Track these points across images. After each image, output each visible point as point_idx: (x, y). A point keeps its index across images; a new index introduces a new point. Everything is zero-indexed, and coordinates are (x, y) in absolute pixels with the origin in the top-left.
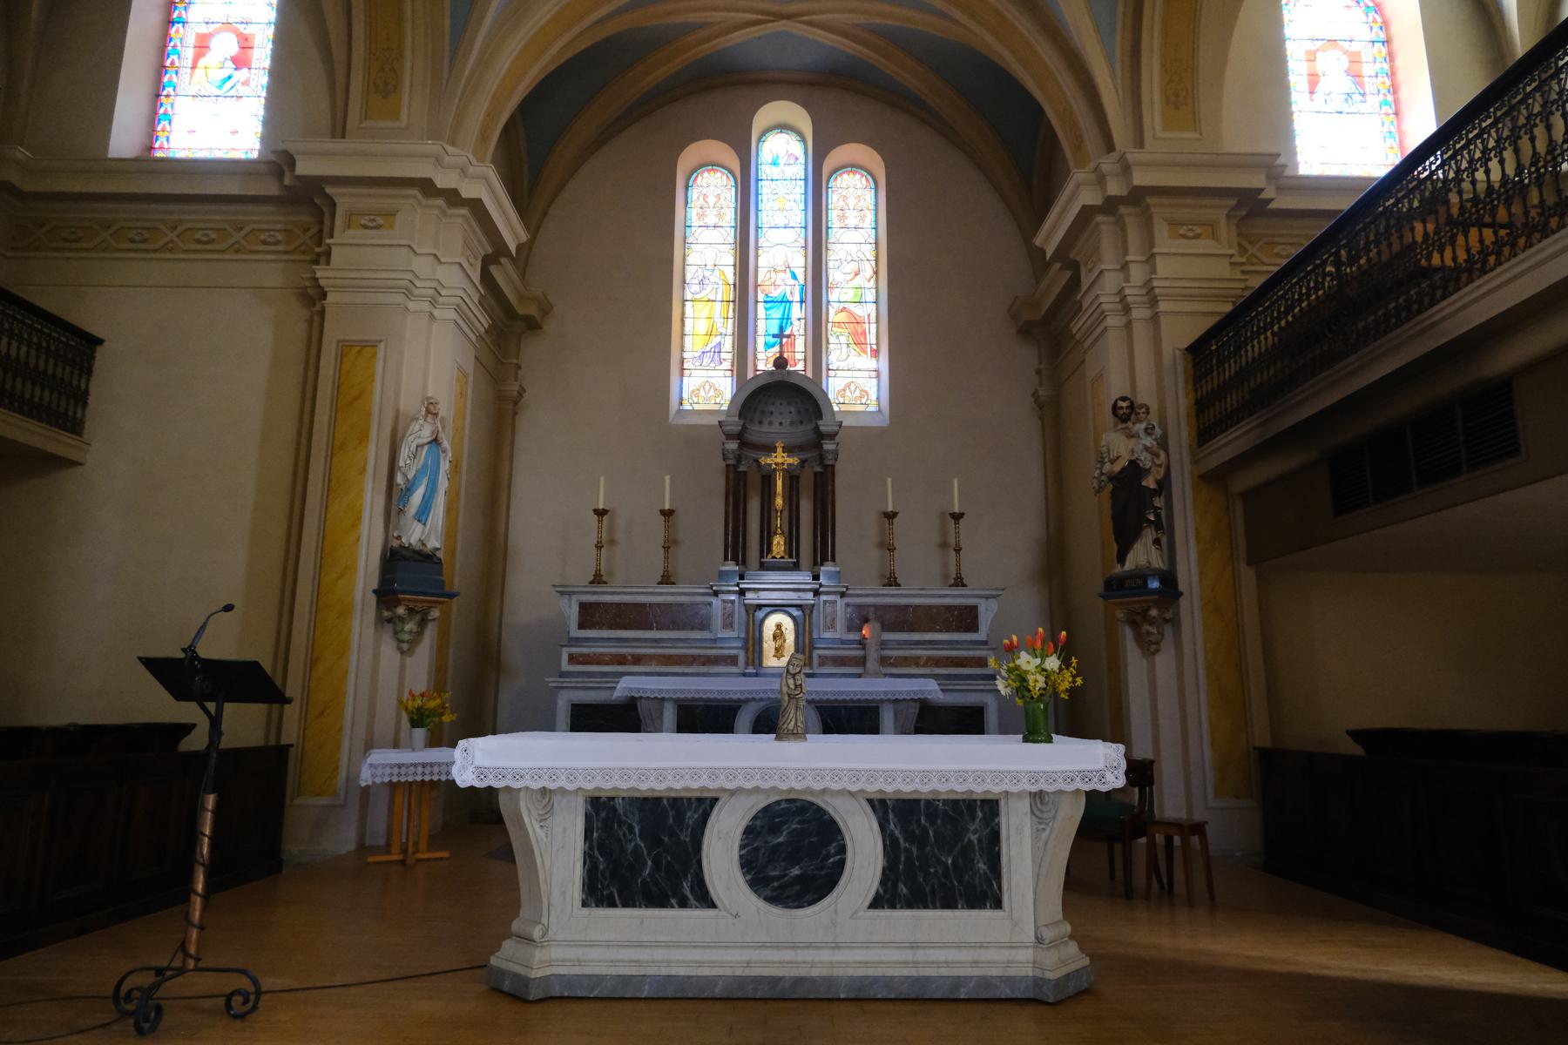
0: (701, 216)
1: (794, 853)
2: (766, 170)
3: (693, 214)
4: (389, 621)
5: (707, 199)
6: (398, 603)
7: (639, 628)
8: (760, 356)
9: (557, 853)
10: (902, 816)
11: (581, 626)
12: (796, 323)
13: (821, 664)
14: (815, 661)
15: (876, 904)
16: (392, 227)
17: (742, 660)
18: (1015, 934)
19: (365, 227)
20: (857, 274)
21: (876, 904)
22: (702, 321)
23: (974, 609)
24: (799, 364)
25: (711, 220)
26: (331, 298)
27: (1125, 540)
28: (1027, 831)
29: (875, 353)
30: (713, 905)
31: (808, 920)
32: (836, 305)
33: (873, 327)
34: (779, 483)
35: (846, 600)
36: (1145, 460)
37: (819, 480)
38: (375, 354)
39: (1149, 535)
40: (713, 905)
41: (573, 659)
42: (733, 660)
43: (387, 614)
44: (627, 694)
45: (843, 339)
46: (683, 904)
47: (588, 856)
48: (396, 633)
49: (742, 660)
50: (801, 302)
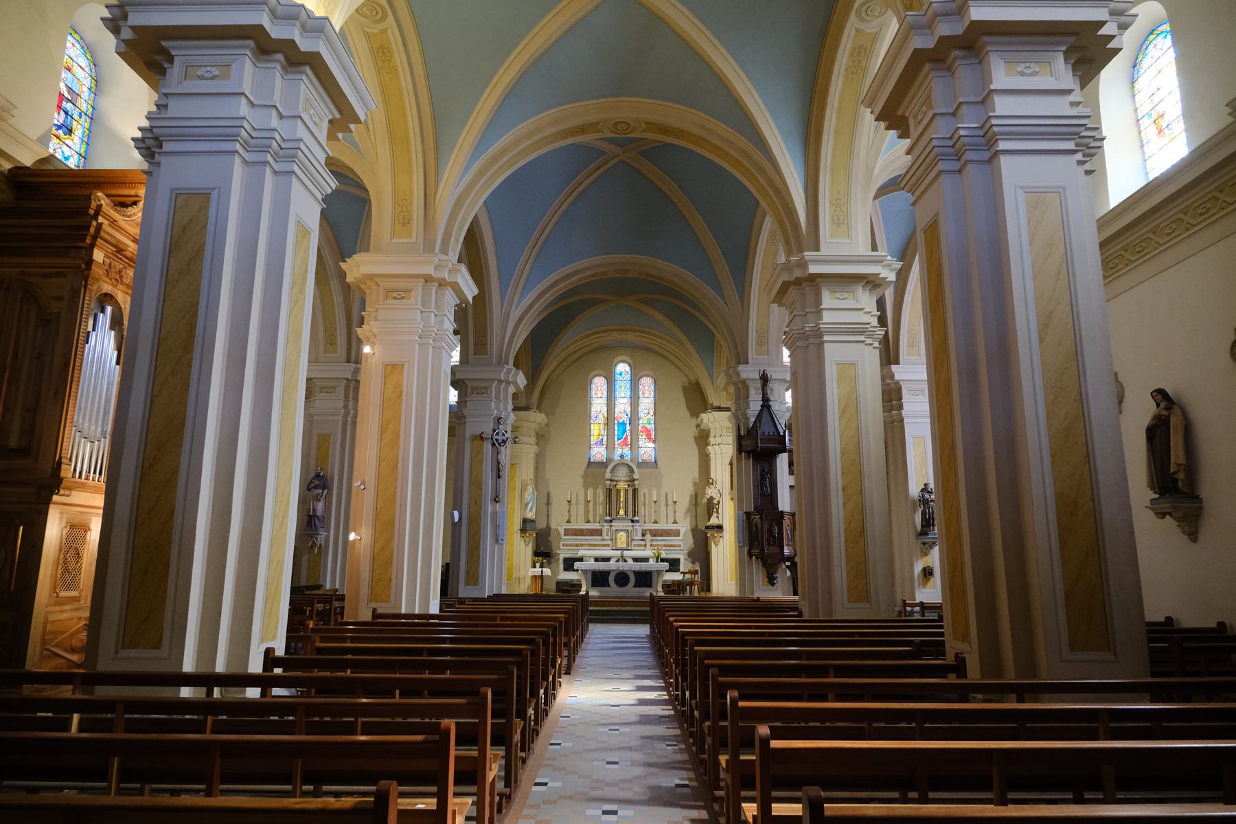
22: (597, 430)
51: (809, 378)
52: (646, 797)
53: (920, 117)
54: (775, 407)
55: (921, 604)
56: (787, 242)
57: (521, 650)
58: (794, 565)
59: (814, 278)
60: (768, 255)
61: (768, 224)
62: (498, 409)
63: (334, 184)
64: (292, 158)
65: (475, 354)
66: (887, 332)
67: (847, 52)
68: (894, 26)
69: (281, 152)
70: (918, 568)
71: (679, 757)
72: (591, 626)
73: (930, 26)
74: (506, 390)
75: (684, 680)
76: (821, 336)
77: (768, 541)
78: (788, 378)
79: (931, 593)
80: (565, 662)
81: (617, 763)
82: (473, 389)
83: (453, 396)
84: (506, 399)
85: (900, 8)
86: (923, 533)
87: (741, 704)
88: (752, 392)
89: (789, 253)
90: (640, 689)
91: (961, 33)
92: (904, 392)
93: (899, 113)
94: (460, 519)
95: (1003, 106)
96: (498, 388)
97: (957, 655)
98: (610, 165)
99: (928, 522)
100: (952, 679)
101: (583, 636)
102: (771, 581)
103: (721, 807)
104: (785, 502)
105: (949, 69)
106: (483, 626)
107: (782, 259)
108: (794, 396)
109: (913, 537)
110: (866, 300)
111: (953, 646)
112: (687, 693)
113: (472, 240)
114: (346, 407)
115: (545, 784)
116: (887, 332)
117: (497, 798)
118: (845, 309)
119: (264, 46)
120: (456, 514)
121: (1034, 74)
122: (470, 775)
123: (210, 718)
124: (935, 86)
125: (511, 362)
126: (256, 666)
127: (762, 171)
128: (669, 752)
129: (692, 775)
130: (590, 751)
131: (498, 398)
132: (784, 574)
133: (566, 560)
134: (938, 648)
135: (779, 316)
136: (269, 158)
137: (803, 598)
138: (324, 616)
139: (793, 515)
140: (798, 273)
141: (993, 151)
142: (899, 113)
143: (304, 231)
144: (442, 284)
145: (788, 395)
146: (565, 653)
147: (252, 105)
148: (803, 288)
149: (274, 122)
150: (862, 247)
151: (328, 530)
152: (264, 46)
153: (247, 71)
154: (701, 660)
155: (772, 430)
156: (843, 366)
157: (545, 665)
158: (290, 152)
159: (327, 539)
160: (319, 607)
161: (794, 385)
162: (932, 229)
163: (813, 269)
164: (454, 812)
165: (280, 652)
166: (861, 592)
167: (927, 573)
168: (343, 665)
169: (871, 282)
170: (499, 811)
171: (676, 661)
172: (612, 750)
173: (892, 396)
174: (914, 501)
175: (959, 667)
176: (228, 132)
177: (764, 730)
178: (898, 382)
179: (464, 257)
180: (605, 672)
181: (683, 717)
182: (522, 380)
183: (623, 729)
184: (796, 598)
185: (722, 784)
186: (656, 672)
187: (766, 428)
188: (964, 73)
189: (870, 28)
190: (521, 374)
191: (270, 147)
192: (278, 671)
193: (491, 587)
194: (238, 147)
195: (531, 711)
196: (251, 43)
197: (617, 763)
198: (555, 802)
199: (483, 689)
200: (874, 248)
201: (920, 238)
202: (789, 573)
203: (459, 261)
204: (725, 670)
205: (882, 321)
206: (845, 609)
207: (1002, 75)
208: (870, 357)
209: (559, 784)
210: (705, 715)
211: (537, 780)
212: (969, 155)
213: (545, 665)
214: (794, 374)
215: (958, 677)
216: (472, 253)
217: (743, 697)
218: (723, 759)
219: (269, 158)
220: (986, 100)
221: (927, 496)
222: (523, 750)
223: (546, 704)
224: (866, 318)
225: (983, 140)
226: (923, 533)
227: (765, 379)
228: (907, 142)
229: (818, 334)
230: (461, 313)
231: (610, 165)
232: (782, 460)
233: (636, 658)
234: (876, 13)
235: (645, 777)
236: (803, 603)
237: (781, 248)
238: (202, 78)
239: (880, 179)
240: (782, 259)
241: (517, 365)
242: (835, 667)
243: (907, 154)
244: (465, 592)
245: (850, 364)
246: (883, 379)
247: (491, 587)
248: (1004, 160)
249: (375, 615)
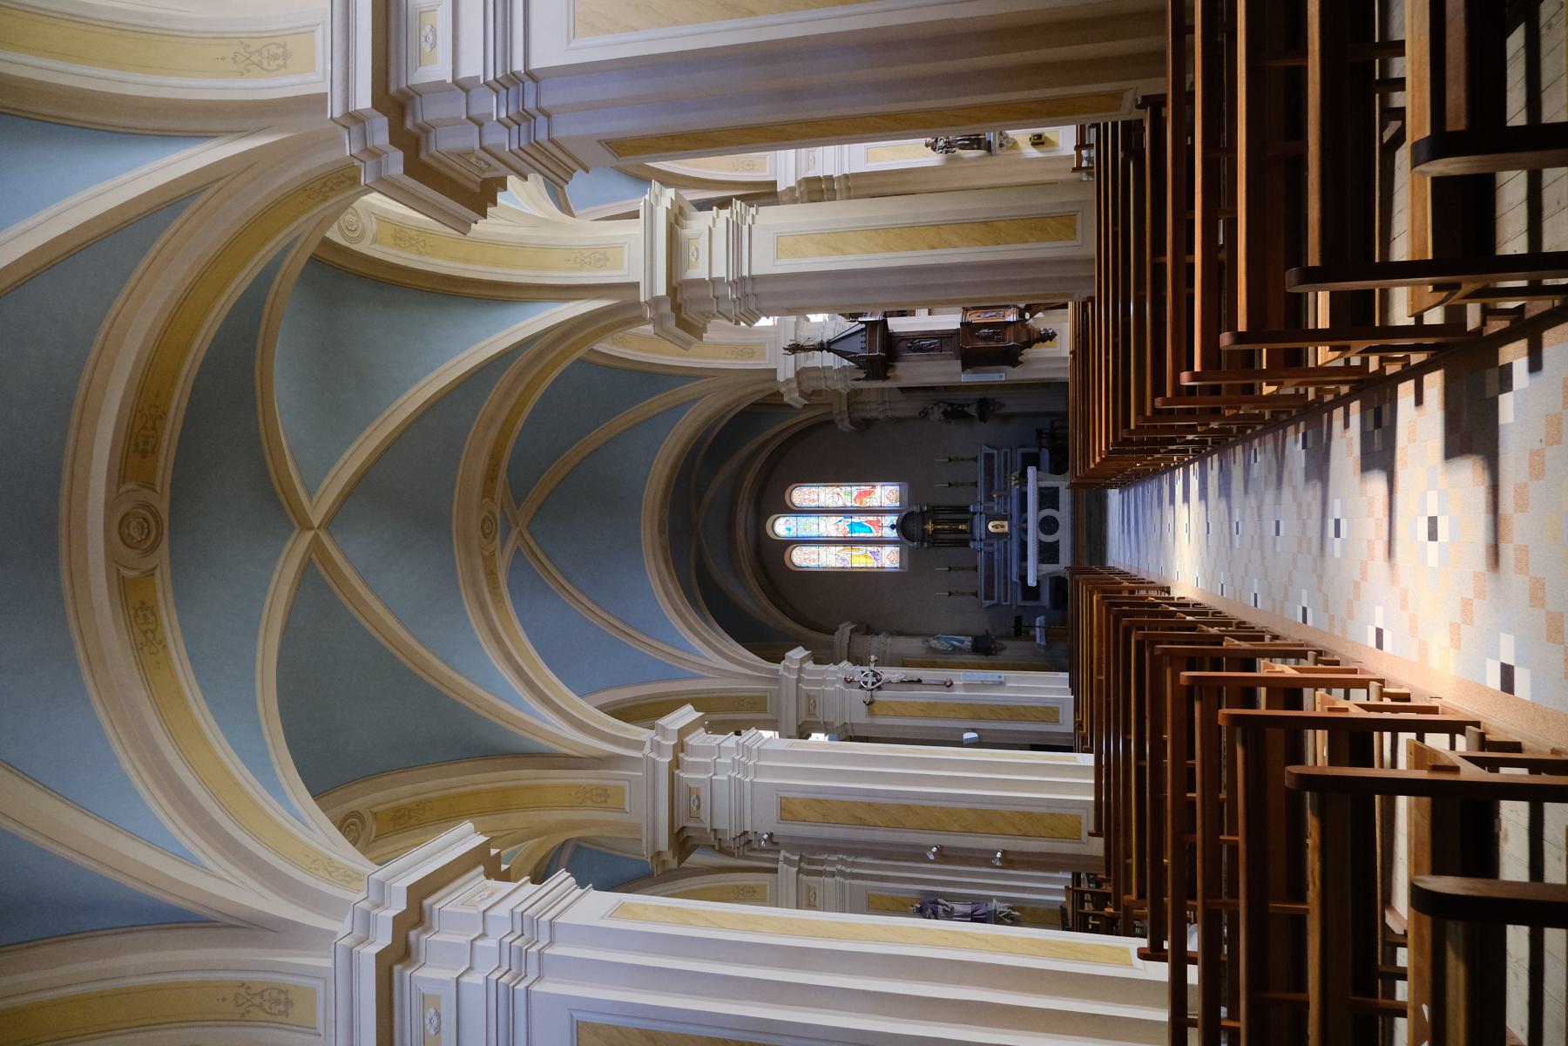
1: (1048, 525)
2: (792, 534)
3: (813, 564)
5: (803, 558)
9: (1049, 568)
10: (1041, 506)
16: (437, 998)
18: (1061, 483)
22: (860, 559)
24: (893, 519)
26: (748, 828)
27: (967, 416)
37: (934, 512)
51: (793, 293)
52: (1319, 485)
53: (483, 165)
54: (829, 335)
55: (1078, 148)
56: (629, 323)
57: (1137, 642)
58: (1028, 308)
59: (673, 289)
60: (641, 346)
61: (604, 346)
62: (834, 682)
63: (563, 874)
64: (535, 923)
65: (765, 711)
66: (738, 198)
67: (400, 253)
68: (376, 200)
69: (527, 935)
70: (1033, 153)
71: (1270, 446)
72: (1110, 563)
73: (375, 154)
74: (810, 673)
75: (1172, 441)
76: (743, 279)
77: (999, 340)
78: (793, 318)
79: (1064, 138)
80: (1154, 593)
81: (1278, 523)
82: (809, 713)
83: (818, 737)
84: (822, 673)
85: (358, 190)
86: (988, 147)
87: (1197, 368)
88: (810, 364)
89: (641, 320)
90: (1186, 498)
91: (386, 119)
92: (811, 174)
93: (478, 190)
94: (974, 730)
95: (472, 67)
96: (810, 682)
97: (1138, 107)
98: (532, 544)
99: (975, 142)
100: (1168, 112)
101: (1120, 573)
102: (1049, 337)
103: (1329, 392)
104: (950, 321)
105: (427, 132)
106: (1108, 695)
107: (649, 329)
108: (816, 310)
109: (991, 160)
110: (698, 223)
111: (1128, 111)
112: (1190, 437)
113: (627, 712)
114: (833, 874)
115: (1305, 610)
116: (738, 198)
117: (1320, 666)
118: (711, 250)
119: (400, 953)
120: (967, 736)
121: (434, 31)
122: (1290, 693)
123: (1224, 1023)
124: (448, 143)
125: (775, 666)
126: (1160, 971)
127: (541, 354)
128: (1262, 460)
129: (1291, 429)
130: (1263, 558)
131: (819, 683)
132: (1040, 321)
133: (1024, 598)
134: (1132, 129)
135: (718, 332)
136: (534, 950)
137: (1070, 296)
138: (1101, 900)
139: (966, 310)
140: (666, 308)
141: (524, 78)
142: (478, 190)
143: (622, 909)
144: (680, 747)
145: (816, 318)
146: (1143, 593)
147: (470, 968)
148: (685, 305)
149: (491, 943)
150: (634, 231)
151: (990, 898)
152: (400, 953)
153: (430, 974)
154: (1147, 419)
155: (859, 338)
156: (779, 251)
157: (1156, 614)
158: (526, 924)
159: (1000, 899)
160: (1088, 907)
161: (802, 311)
162: (621, 147)
163: (661, 290)
164: (1330, 710)
165: (1144, 943)
166: (1064, 224)
167: (1038, 141)
168: (1158, 869)
169: (676, 219)
170: (1337, 663)
171: (1151, 452)
172: (1261, 529)
173: (816, 190)
174: (948, 160)
175: (1154, 103)
176: (504, 1000)
177: (1225, 339)
178: (799, 183)
179: (649, 723)
180: (1161, 543)
181: (1220, 443)
182: (798, 653)
183: (1237, 518)
184: (1070, 304)
185: (1302, 391)
186: (1166, 478)
187: (856, 346)
188: (430, 112)
189: (372, 226)
190: (789, 654)
191: (520, 949)
192: (1166, 945)
193: (1060, 691)
194: (521, 986)
195: (1215, 630)
196: (397, 968)
197: (1278, 523)
198: (1326, 598)
199: (1183, 682)
200: (634, 215)
201: (628, 162)
202: (1040, 315)
203: (652, 728)
204: (1159, 390)
205: (724, 203)
206: (1085, 243)
207: (433, 68)
208: (768, 218)
209: (1304, 592)
210: (1216, 412)
211: (1300, 619)
212: (530, 104)
213: (1156, 614)
214: (790, 311)
215: (1165, 105)
216: (643, 712)
217: (1190, 367)
218: (1268, 390)
219: (534, 950)
220: (463, 87)
221: (941, 143)
222: (1262, 639)
223: (1206, 614)
224: (721, 224)
225: (512, 90)
226: (988, 147)
227: (795, 348)
228: (512, 180)
229: (740, 282)
230: (716, 728)
231: (532, 544)
232: (897, 325)
233: (1148, 499)
234: (354, 219)
235: (1295, 488)
236: (1076, 296)
237: (634, 330)
238: (438, 1030)
239: (549, 209)
240: (649, 329)
241: (778, 659)
242: (1153, 255)
243: (526, 178)
244: (1066, 725)
245: (780, 241)
246: (795, 201)
247: (1060, 691)
248: (535, 64)
249: (1097, 833)
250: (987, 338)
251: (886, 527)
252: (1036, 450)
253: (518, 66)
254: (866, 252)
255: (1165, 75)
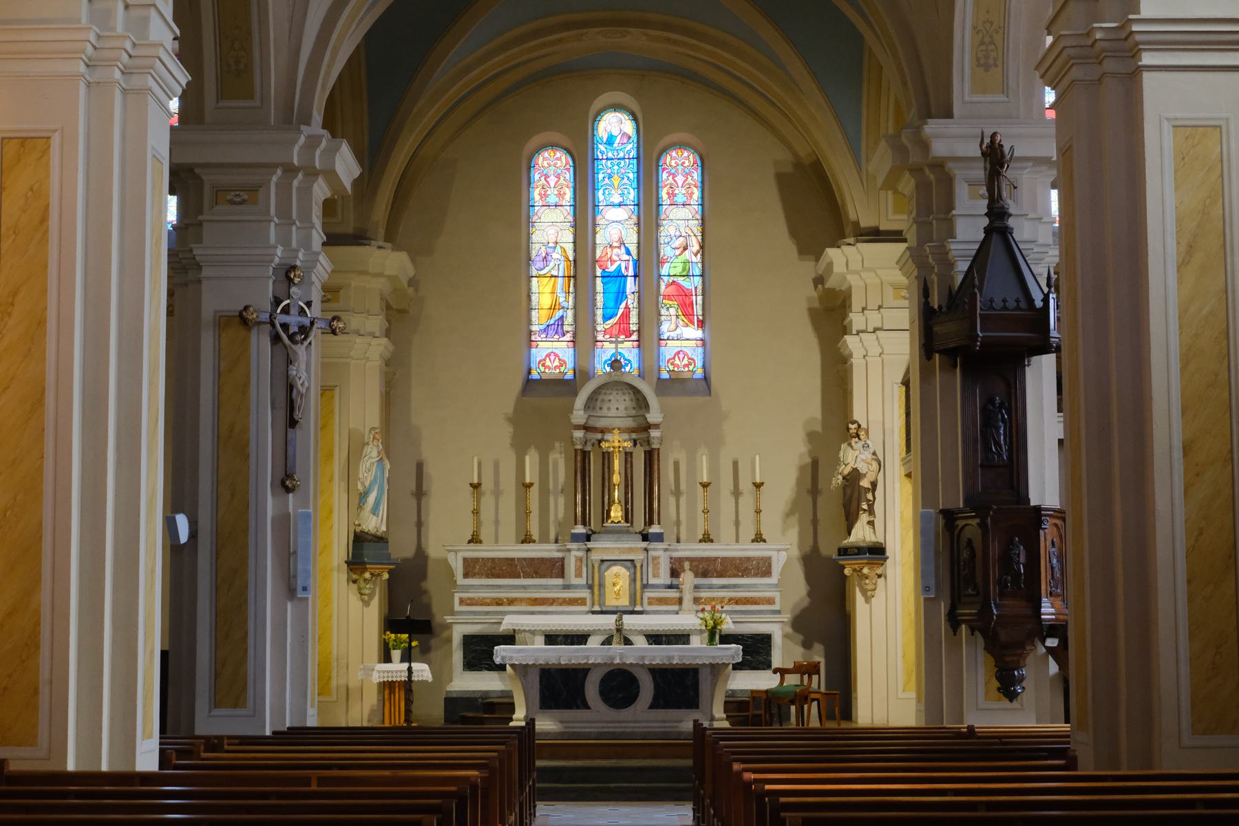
0: (544, 196)
4: (355, 582)
5: (551, 171)
6: (365, 570)
7: (511, 577)
8: (599, 328)
11: (466, 575)
12: (630, 297)
13: (650, 604)
14: (645, 601)
15: (651, 707)
17: (589, 602)
19: (232, 202)
20: (685, 249)
21: (651, 707)
22: (547, 294)
23: (770, 558)
25: (552, 199)
26: (206, 272)
28: (709, 679)
29: (701, 324)
30: (589, 708)
31: (626, 713)
32: (666, 279)
33: (700, 298)
34: (616, 463)
35: (668, 553)
36: (862, 468)
38: (333, 397)
39: (864, 518)
40: (589, 708)
41: (462, 601)
42: (582, 602)
43: (355, 577)
44: (511, 628)
45: (672, 311)
46: (578, 708)
47: (541, 691)
48: (359, 589)
49: (589, 602)
50: (635, 276)
54: (1022, 230)
62: (286, 243)
74: (306, 191)
76: (1135, 53)
77: (1001, 583)
78: (1052, 151)
82: (219, 191)
84: (306, 216)
88: (962, 192)
94: (193, 535)
96: (285, 188)
102: (1008, 686)
104: (1045, 484)
120: (182, 522)
125: (318, 117)
131: (284, 213)
132: (1040, 668)
133: (469, 641)
139: (1060, 514)
156: (1193, 134)
187: (998, 290)
202: (1053, 668)
227: (995, 158)
232: (1041, 375)
244: (210, 722)
248: (1147, 77)
250: (1007, 560)
251: (615, 351)
252: (777, 662)
253: (1147, 59)
254: (1183, 312)
255: (1095, 770)
